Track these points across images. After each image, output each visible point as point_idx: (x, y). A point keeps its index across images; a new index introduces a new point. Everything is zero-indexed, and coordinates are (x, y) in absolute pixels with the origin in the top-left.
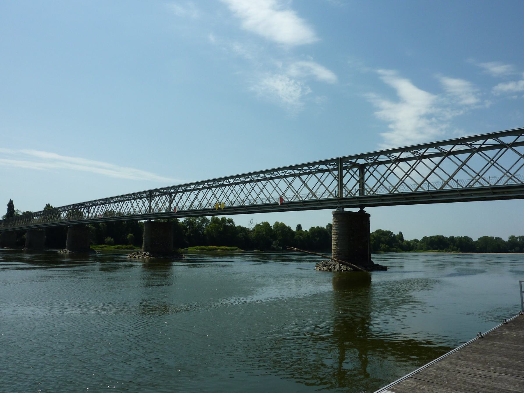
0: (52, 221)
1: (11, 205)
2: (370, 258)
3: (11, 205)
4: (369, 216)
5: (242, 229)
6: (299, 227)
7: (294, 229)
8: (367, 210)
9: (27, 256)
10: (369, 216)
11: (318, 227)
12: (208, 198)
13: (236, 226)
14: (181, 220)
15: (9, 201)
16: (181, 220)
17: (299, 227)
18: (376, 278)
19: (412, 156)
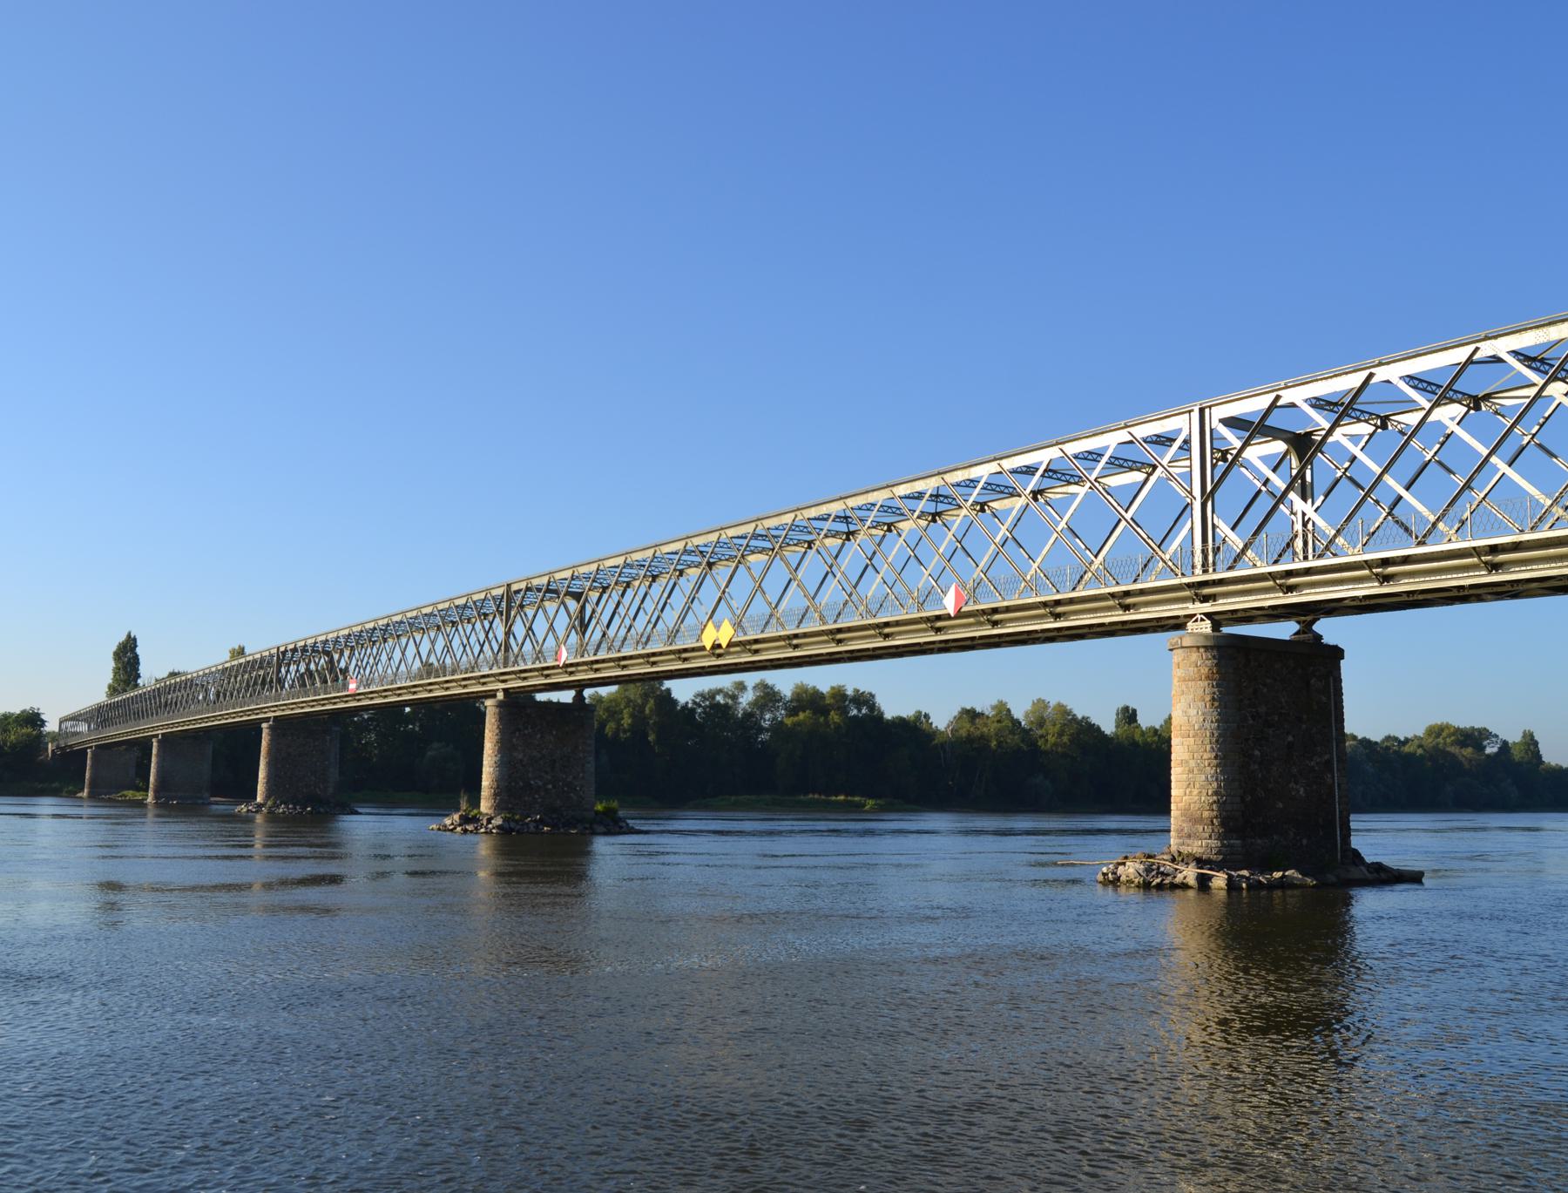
0: (1220, 700)
1: (127, 657)
2: (1347, 832)
3: (127, 657)
4: (1337, 653)
5: (913, 730)
6: (1128, 716)
7: (1108, 726)
8: (1329, 630)
9: (85, 811)
10: (1337, 653)
11: (971, 715)
12: (737, 604)
13: (888, 715)
14: (408, 709)
15: (123, 638)
16: (408, 709)
17: (1128, 716)
18: (1367, 903)
19: (895, 489)
